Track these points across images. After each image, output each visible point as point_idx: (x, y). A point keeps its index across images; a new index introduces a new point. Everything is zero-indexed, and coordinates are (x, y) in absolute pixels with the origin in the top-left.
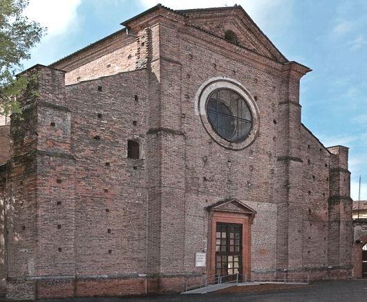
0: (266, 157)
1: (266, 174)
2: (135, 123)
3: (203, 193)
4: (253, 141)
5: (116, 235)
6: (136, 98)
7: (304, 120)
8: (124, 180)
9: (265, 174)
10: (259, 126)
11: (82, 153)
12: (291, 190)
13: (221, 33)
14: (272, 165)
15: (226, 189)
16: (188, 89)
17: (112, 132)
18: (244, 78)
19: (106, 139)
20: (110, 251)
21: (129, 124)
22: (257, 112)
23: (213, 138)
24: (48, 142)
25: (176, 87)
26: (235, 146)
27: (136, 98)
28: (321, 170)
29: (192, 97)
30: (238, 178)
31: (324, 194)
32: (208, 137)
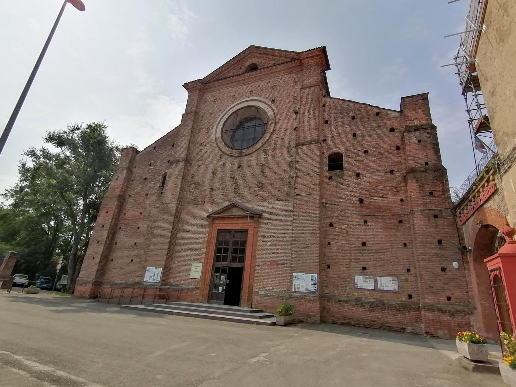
3: (208, 203)
5: (138, 247)
15: (233, 194)
20: (132, 260)
23: (223, 152)
26: (245, 152)
30: (247, 180)
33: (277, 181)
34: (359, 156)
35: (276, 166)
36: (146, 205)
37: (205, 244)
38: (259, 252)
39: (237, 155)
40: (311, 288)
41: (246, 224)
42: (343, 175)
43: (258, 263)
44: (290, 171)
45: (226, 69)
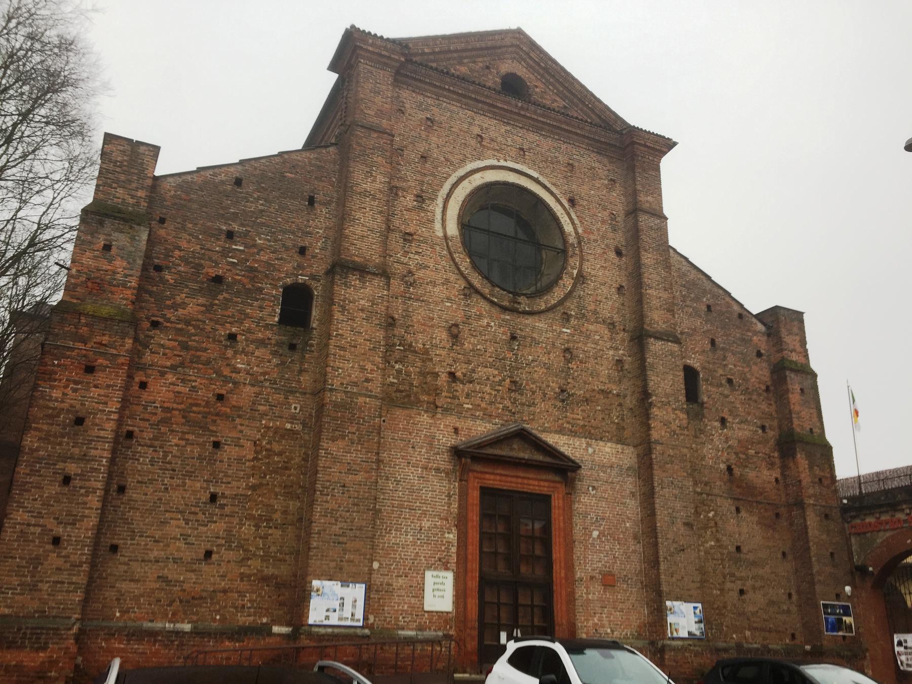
1: (604, 370)
2: (302, 251)
3: (447, 411)
4: (571, 292)
5: (227, 510)
6: (311, 201)
7: (678, 238)
8: (264, 374)
10: (582, 259)
11: (181, 311)
12: (655, 411)
14: (617, 349)
15: (507, 403)
16: (422, 183)
17: (252, 269)
18: (544, 163)
19: (236, 282)
20: (208, 554)
22: (575, 229)
24: (90, 284)
25: (380, 178)
26: (524, 304)
27: (311, 201)
28: (749, 366)
29: (430, 199)
30: (536, 376)
31: (763, 428)
33: (597, 396)
34: (721, 385)
35: (592, 361)
36: (238, 371)
37: (452, 521)
38: (578, 550)
39: (506, 303)
40: (696, 629)
41: (514, 480)
42: (703, 416)
43: (578, 575)
44: (620, 381)
45: (456, 51)
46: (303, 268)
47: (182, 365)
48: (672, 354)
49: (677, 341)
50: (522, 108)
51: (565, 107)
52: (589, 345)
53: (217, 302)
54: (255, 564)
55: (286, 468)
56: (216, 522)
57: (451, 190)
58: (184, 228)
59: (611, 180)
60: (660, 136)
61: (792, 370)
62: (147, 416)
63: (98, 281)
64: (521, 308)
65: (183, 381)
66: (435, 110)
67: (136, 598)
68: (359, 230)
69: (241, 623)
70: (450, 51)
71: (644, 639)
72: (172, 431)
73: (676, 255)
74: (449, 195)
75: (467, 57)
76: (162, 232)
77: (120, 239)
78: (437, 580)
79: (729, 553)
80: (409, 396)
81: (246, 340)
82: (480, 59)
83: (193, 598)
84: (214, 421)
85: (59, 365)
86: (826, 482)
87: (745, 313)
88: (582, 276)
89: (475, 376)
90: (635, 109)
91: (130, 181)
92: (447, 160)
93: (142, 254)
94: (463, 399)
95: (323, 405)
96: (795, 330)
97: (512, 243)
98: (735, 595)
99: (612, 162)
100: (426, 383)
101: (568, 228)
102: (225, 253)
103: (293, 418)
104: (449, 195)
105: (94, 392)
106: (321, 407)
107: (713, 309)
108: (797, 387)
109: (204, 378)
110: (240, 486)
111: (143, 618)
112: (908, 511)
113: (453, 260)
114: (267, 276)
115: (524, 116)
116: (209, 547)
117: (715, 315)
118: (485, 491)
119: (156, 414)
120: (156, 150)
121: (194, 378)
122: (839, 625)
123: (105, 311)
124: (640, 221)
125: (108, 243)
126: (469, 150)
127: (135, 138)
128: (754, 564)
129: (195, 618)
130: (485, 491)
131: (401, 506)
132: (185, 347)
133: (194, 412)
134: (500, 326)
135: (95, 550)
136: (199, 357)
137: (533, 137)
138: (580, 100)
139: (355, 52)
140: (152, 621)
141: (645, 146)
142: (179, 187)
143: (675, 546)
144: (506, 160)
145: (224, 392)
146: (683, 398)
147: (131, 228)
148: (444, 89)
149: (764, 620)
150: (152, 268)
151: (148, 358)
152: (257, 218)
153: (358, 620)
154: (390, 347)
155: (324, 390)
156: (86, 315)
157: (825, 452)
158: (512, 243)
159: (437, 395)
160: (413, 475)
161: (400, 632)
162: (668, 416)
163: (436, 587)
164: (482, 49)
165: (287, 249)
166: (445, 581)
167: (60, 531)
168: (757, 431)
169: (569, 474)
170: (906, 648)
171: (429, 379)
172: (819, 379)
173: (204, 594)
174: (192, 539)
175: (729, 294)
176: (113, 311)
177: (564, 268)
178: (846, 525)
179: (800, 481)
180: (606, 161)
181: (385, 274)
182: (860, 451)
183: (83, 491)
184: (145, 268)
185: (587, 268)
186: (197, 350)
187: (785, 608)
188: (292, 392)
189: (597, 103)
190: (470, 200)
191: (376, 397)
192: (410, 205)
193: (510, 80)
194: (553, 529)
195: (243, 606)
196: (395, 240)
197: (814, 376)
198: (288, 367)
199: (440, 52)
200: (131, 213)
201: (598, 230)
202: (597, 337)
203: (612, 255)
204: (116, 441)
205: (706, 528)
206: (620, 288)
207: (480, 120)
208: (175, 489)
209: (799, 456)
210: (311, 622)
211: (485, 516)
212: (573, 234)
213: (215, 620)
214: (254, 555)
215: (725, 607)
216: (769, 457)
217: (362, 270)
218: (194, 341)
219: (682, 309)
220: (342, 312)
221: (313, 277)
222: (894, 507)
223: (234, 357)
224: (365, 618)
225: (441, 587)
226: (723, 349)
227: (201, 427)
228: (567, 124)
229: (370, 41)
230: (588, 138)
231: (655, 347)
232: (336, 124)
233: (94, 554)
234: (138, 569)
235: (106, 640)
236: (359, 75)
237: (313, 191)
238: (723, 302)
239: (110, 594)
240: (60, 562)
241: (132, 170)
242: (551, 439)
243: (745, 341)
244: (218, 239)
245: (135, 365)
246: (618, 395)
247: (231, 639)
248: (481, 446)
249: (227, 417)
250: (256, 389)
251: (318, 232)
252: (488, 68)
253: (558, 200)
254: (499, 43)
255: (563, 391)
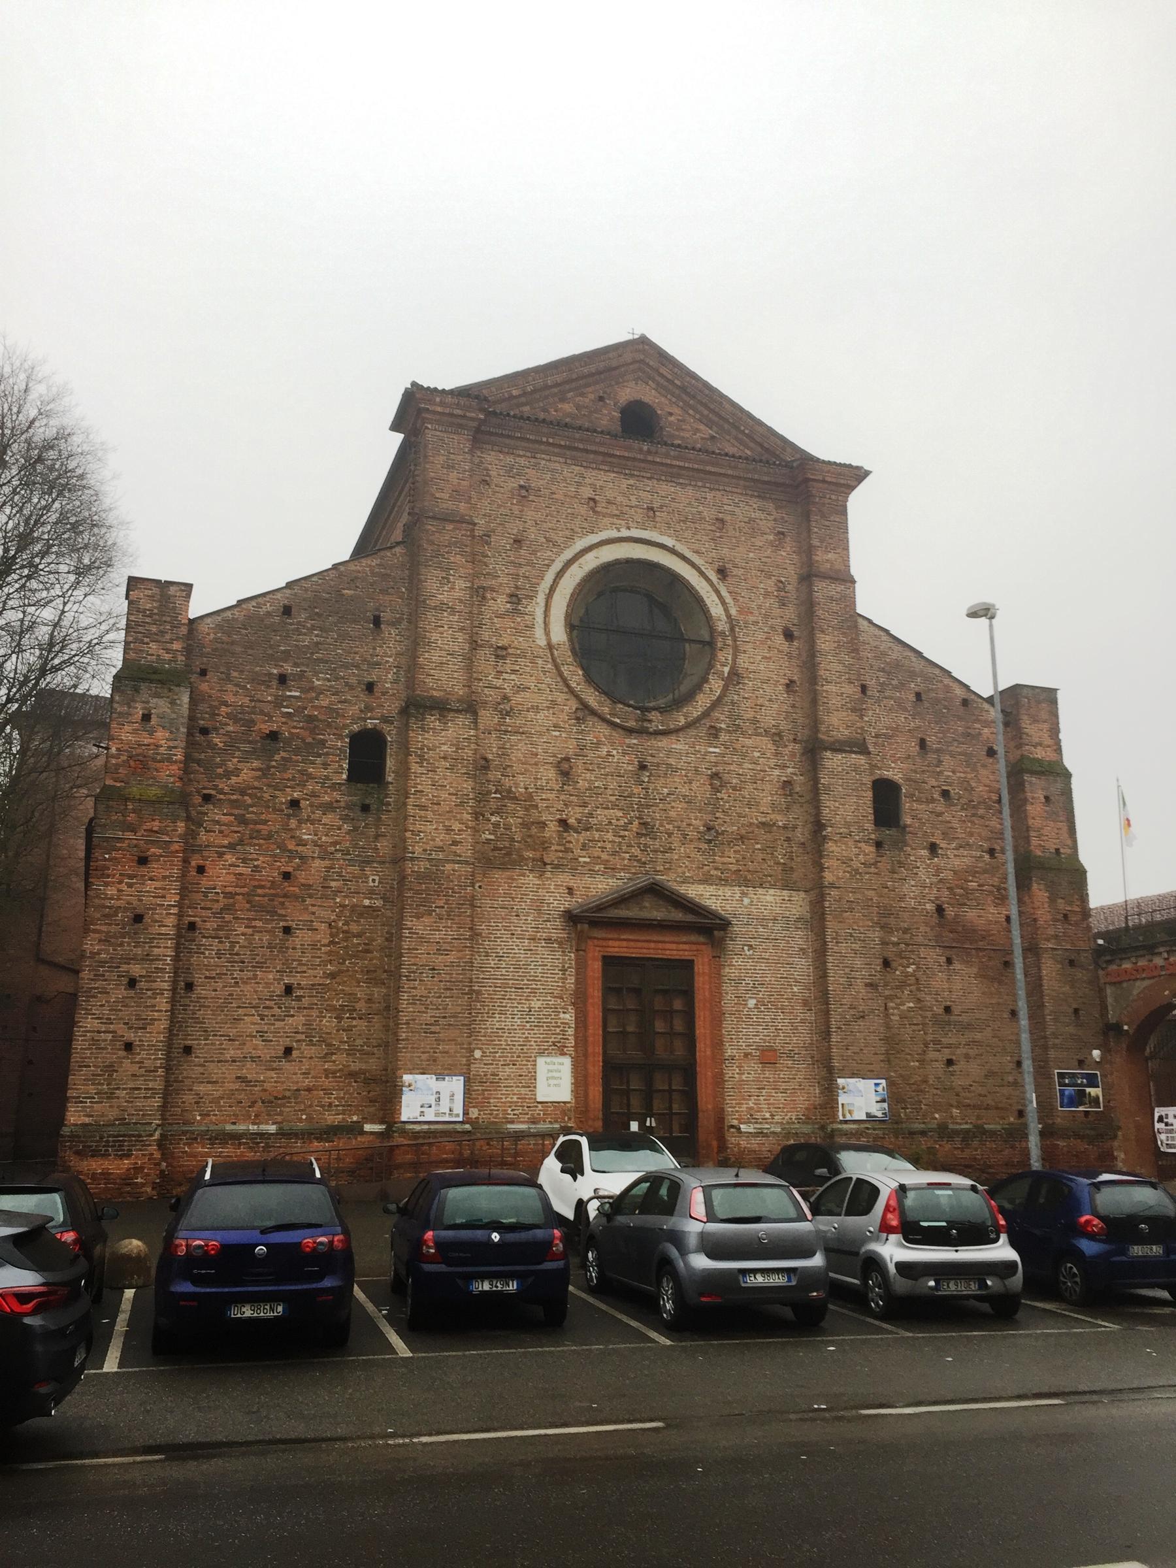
0: (766, 744)
1: (767, 796)
2: (370, 687)
5: (305, 1002)
8: (335, 844)
9: (766, 800)
11: (234, 780)
12: (830, 846)
13: (608, 417)
15: (636, 851)
16: (516, 577)
17: (311, 719)
20: (288, 1051)
21: (291, 708)
22: (726, 610)
24: (132, 763)
26: (656, 721)
27: (377, 621)
28: (974, 770)
30: (673, 814)
32: (574, 704)
34: (933, 800)
36: (302, 843)
38: (728, 1024)
39: (631, 724)
40: (877, 1110)
41: (645, 945)
43: (729, 1053)
45: (557, 385)
46: (371, 710)
47: (241, 842)
48: (856, 769)
49: (864, 751)
50: (649, 452)
51: (713, 437)
52: (746, 765)
53: (274, 763)
54: (340, 1059)
55: (367, 951)
56: (293, 1016)
57: (555, 581)
58: (228, 678)
59: (780, 533)
60: (845, 465)
61: (1033, 773)
62: (209, 904)
63: (140, 758)
64: (652, 727)
65: (244, 861)
66: (531, 472)
67: (216, 1101)
68: (435, 656)
69: (329, 1123)
70: (547, 387)
71: (814, 1123)
72: (237, 918)
73: (872, 628)
74: (552, 589)
75: (570, 390)
76: (204, 687)
77: (160, 706)
78: (551, 1067)
79: (934, 1015)
80: (509, 854)
81: (311, 805)
82: (590, 389)
83: (276, 1098)
84: (283, 904)
85: (110, 860)
86: (1073, 919)
87: (973, 697)
88: (737, 675)
89: (593, 821)
90: (813, 428)
91: (163, 633)
92: (548, 540)
93: (185, 721)
94: (577, 852)
95: (404, 878)
96: (1044, 715)
97: (639, 639)
98: (940, 1066)
99: (781, 507)
100: (530, 836)
101: (716, 610)
102: (278, 703)
103: (371, 893)
104: (552, 589)
105: (150, 886)
106: (403, 878)
107: (924, 697)
108: (1040, 795)
109: (265, 856)
110: (316, 975)
111: (225, 1122)
112: (1166, 955)
113: (561, 674)
114: (329, 725)
115: (654, 463)
116: (288, 1042)
117: (926, 705)
118: (609, 962)
119: (218, 901)
120: (188, 587)
121: (255, 856)
122: (1080, 1097)
123: (154, 792)
124: (817, 583)
125: (146, 712)
126: (578, 522)
127: (163, 578)
128: (969, 1027)
129: (279, 1118)
130: (609, 962)
131: (505, 986)
132: (242, 820)
133: (259, 896)
134: (624, 754)
135: (169, 1052)
136: (258, 831)
137: (666, 488)
138: (733, 425)
139: (417, 411)
140: (234, 1123)
141: (824, 481)
142: (219, 627)
143: (852, 1012)
144: (629, 528)
145: (290, 869)
146: (870, 826)
147: (170, 690)
148: (541, 443)
149: (980, 1095)
150: (198, 731)
151: (203, 837)
152: (312, 654)
153: (458, 1115)
154: (482, 797)
155: (404, 859)
156: (133, 800)
157: (1077, 877)
158: (639, 639)
159: (545, 849)
160: (518, 948)
161: (509, 1126)
162: (849, 849)
163: (550, 1074)
164: (592, 375)
165: (352, 688)
166: (561, 1067)
167: (130, 1036)
168: (981, 857)
169: (716, 933)
170: (1167, 1124)
171: (534, 830)
172: (1074, 781)
173: (288, 1094)
174: (270, 1036)
175: (948, 673)
176: (159, 792)
177: (711, 666)
178: (1101, 972)
179: (1035, 920)
180: (771, 506)
181: (471, 708)
182: (1120, 874)
183: (149, 993)
184: (190, 734)
185: (743, 662)
186: (256, 823)
187: (1011, 1079)
188: (368, 862)
189: (757, 428)
190: (581, 591)
191: (467, 863)
192: (502, 610)
193: (628, 412)
194: (696, 1001)
195: (330, 1105)
196: (485, 661)
197: (1068, 775)
198: (362, 833)
199: (534, 391)
200: (168, 671)
201: (760, 607)
202: (757, 754)
203: (779, 639)
204: (179, 936)
205: (902, 985)
206: (790, 686)
207: (591, 476)
208: (246, 983)
209: (1035, 886)
210: (404, 1118)
211: (609, 990)
212: (724, 617)
213: (301, 1120)
214: (338, 1049)
215: (926, 1082)
216: (998, 890)
217: (441, 707)
218: (253, 813)
219: (878, 701)
220: (420, 764)
221: (385, 720)
222: (1150, 949)
223: (299, 827)
224: (466, 1113)
225: (555, 1074)
226: (938, 751)
227: (268, 912)
228: (713, 464)
229: (438, 399)
230: (745, 479)
231: (833, 761)
232: (401, 515)
233: (168, 1058)
234: (215, 1071)
235: (189, 1145)
236: (426, 446)
237: (377, 609)
238: (940, 685)
239: (189, 1098)
240: (135, 1068)
241: (164, 619)
242: (695, 892)
243: (970, 736)
244: (268, 687)
245: (190, 847)
246: (785, 827)
247: (319, 1139)
248: (600, 908)
249: (296, 897)
250: (327, 863)
251: (387, 662)
252: (601, 399)
253: (702, 573)
254: (614, 363)
255: (709, 829)
